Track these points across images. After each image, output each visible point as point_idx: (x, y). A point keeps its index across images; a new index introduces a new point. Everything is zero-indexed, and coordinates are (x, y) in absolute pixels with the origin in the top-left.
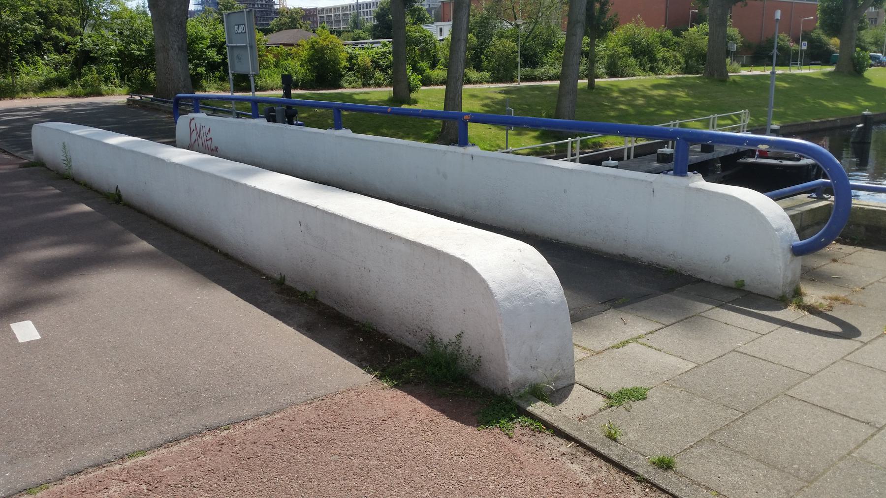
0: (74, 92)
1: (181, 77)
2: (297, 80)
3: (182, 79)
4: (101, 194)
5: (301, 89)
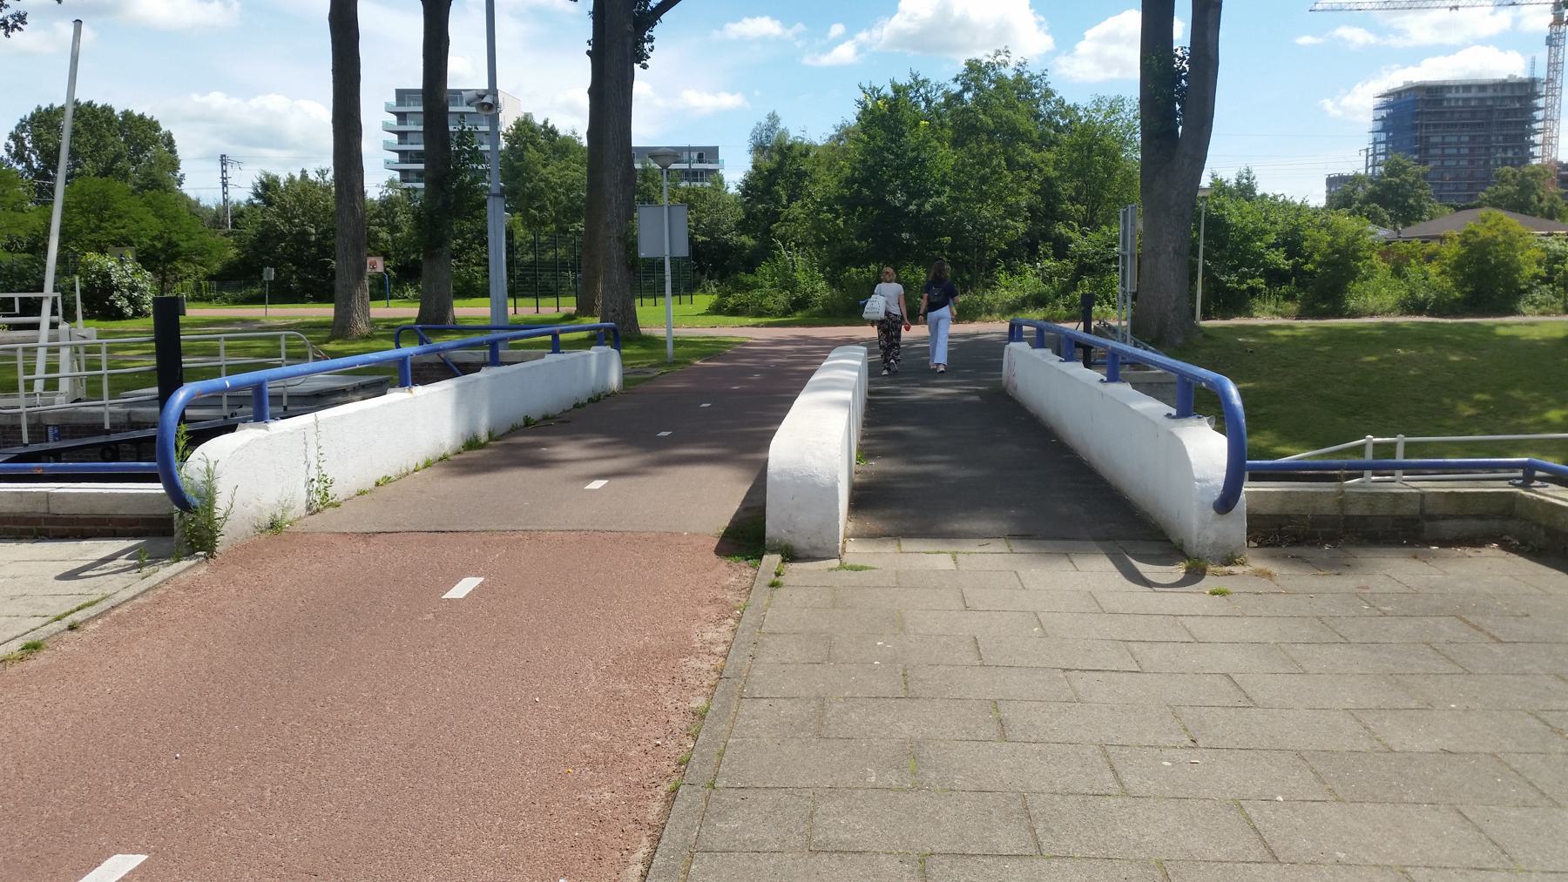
0: (1052, 315)
1: (1173, 294)
2: (1426, 300)
3: (1174, 299)
4: (325, 327)
5: (1431, 314)
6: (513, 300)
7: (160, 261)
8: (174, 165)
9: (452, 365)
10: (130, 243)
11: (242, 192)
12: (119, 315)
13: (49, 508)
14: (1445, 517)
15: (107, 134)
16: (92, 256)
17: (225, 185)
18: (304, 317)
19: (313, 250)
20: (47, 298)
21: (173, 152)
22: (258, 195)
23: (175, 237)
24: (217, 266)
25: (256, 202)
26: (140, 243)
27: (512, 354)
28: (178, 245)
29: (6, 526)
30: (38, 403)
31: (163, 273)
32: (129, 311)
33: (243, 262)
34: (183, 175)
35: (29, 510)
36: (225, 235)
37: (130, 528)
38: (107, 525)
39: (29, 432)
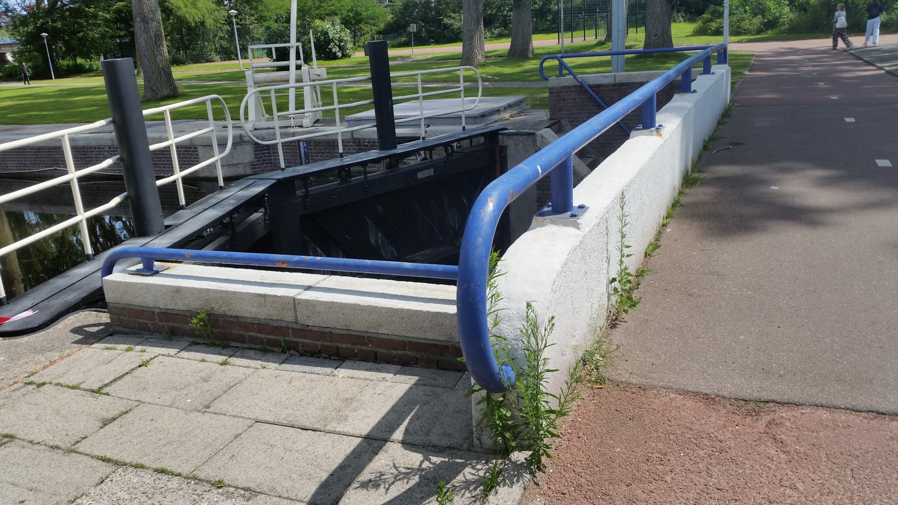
7: (352, 24)
9: (587, 87)
10: (336, 14)
12: (334, 57)
13: (296, 317)
16: (318, 22)
18: (434, 54)
19: (433, 13)
20: (292, 47)
23: (359, 10)
26: (342, 14)
27: (639, 75)
28: (361, 14)
29: (250, 334)
30: (292, 125)
31: (354, 32)
32: (339, 54)
33: (395, 22)
35: (274, 317)
36: (385, 7)
37: (395, 352)
38: (366, 345)
39: (285, 159)
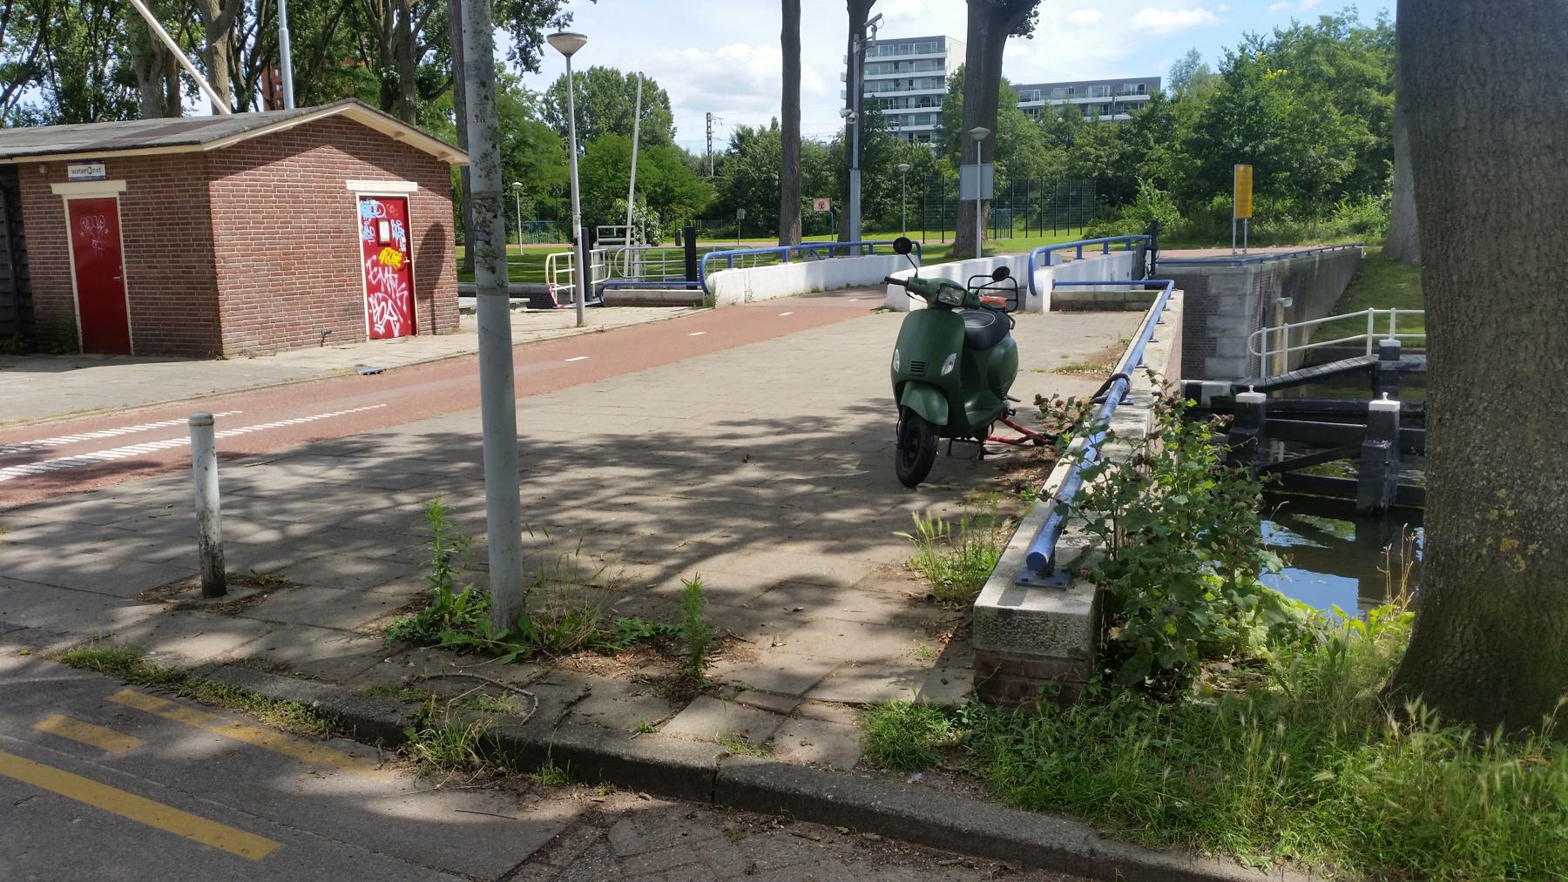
6: (992, 231)
8: (669, 120)
11: (722, 145)
14: (1134, 301)
15: (617, 94)
17: (709, 139)
21: (667, 108)
22: (735, 146)
23: (671, 184)
24: (703, 207)
25: (733, 151)
28: (673, 191)
33: (722, 204)
34: (675, 129)
36: (709, 182)
